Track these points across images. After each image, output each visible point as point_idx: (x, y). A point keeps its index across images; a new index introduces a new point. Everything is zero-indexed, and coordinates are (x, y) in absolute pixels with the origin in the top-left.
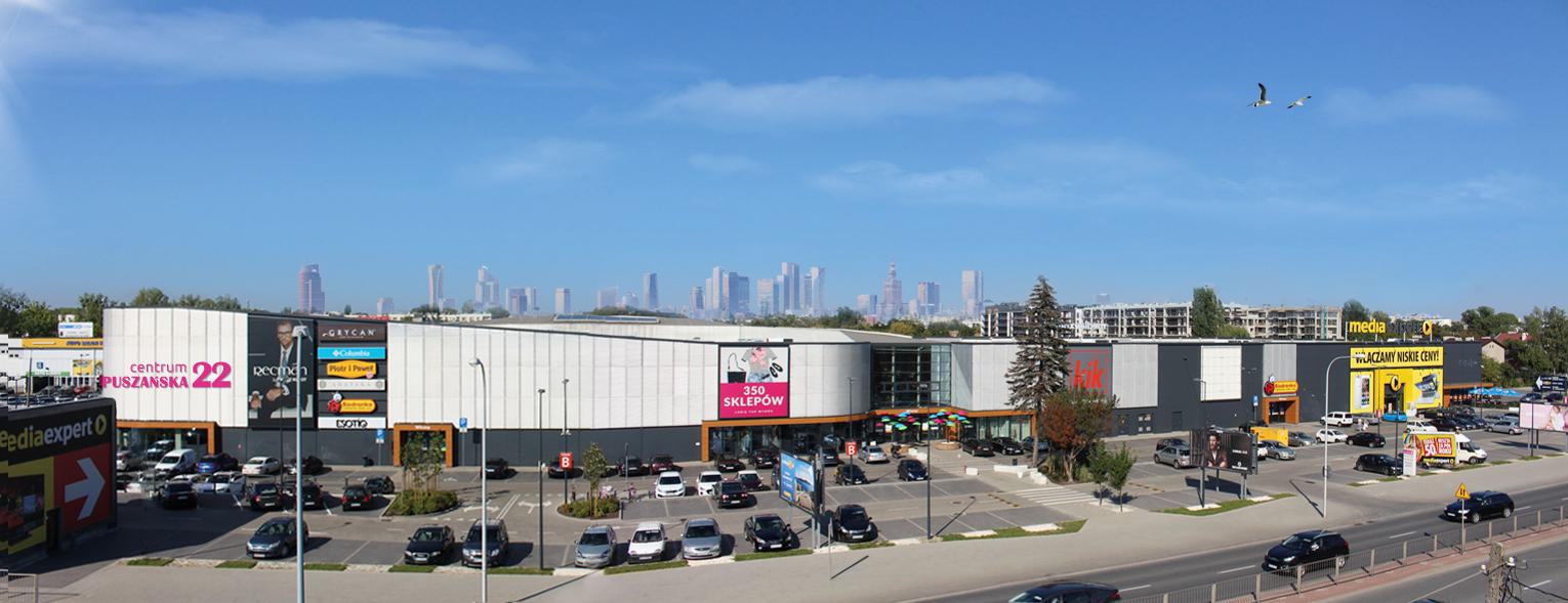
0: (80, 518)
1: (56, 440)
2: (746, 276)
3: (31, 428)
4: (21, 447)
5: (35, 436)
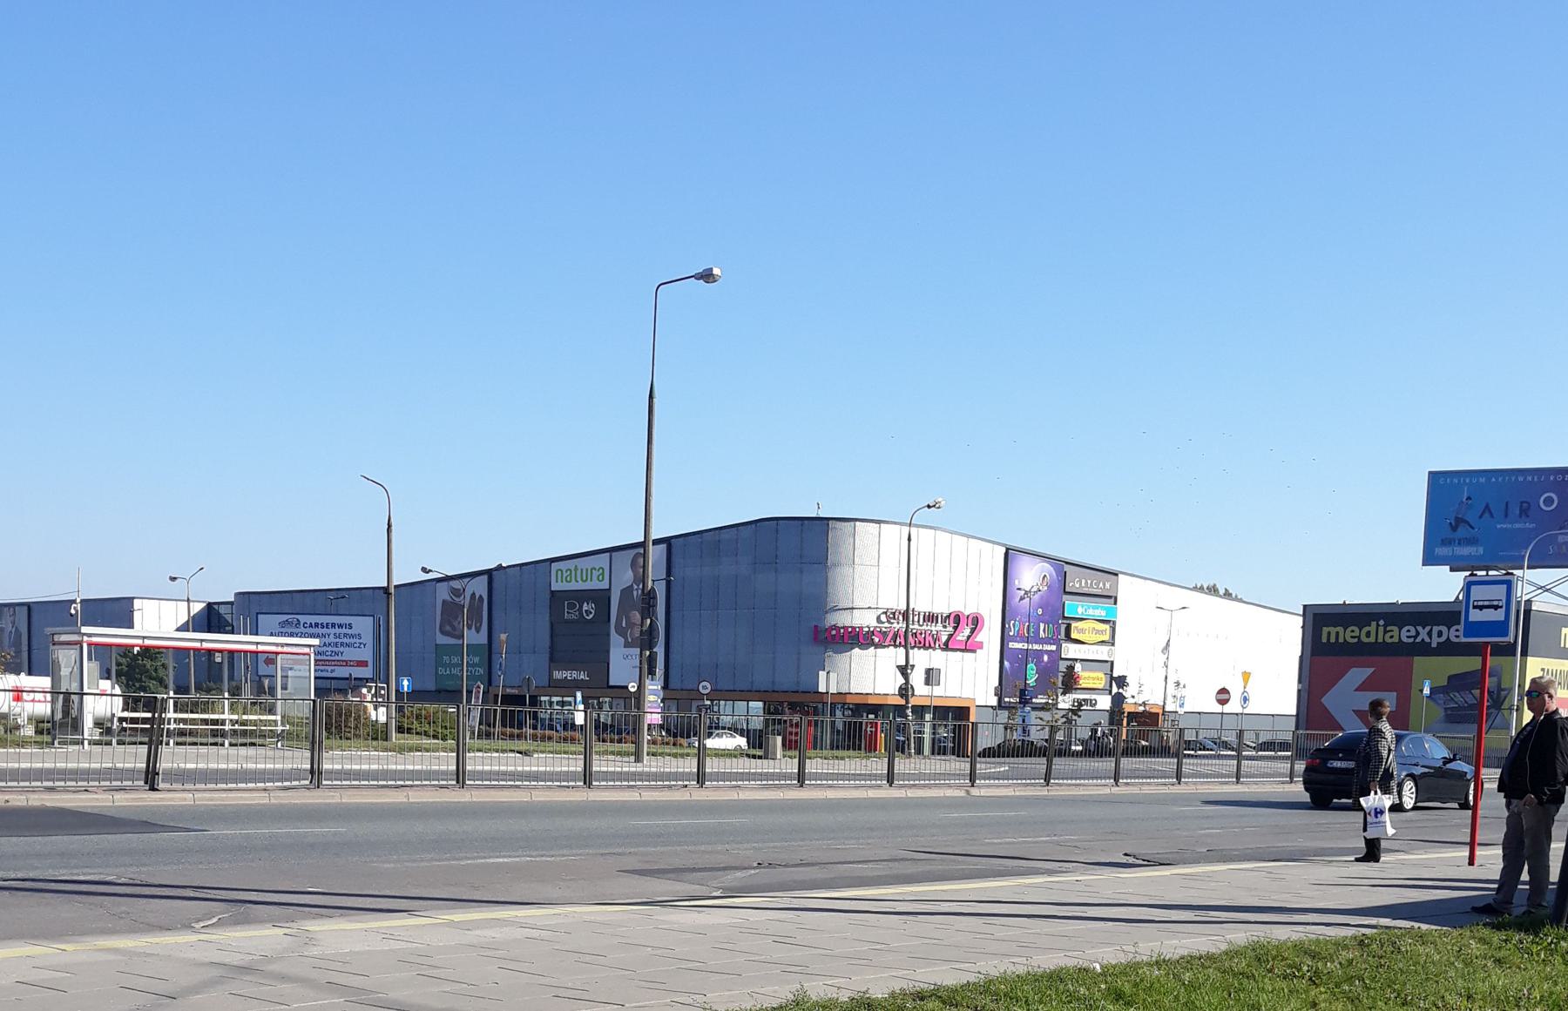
0: (1373, 669)
1: (1418, 640)
2: (923, 672)
3: (1382, 622)
4: (1365, 640)
5: (1385, 632)
